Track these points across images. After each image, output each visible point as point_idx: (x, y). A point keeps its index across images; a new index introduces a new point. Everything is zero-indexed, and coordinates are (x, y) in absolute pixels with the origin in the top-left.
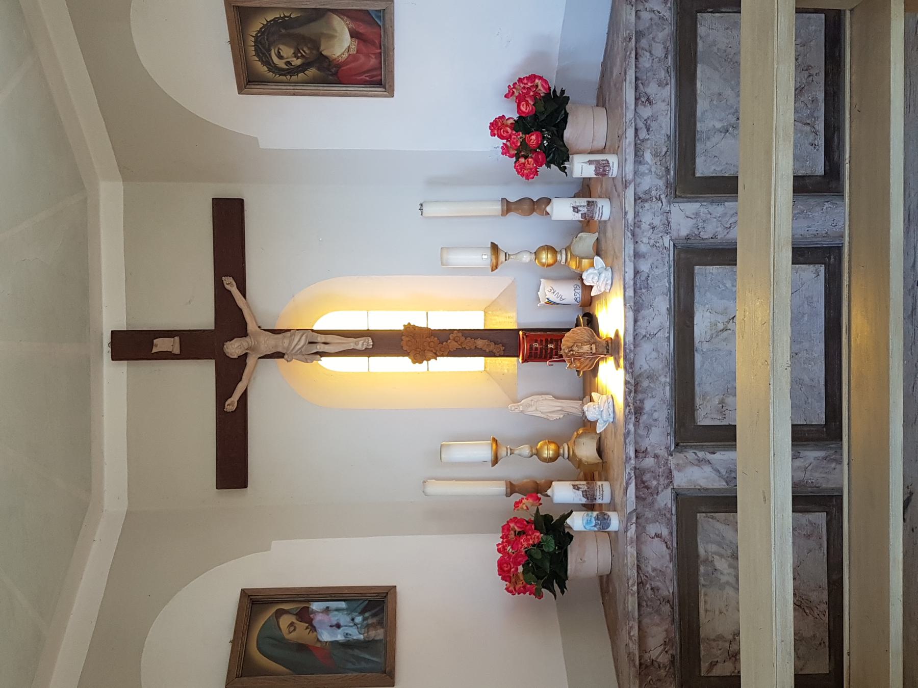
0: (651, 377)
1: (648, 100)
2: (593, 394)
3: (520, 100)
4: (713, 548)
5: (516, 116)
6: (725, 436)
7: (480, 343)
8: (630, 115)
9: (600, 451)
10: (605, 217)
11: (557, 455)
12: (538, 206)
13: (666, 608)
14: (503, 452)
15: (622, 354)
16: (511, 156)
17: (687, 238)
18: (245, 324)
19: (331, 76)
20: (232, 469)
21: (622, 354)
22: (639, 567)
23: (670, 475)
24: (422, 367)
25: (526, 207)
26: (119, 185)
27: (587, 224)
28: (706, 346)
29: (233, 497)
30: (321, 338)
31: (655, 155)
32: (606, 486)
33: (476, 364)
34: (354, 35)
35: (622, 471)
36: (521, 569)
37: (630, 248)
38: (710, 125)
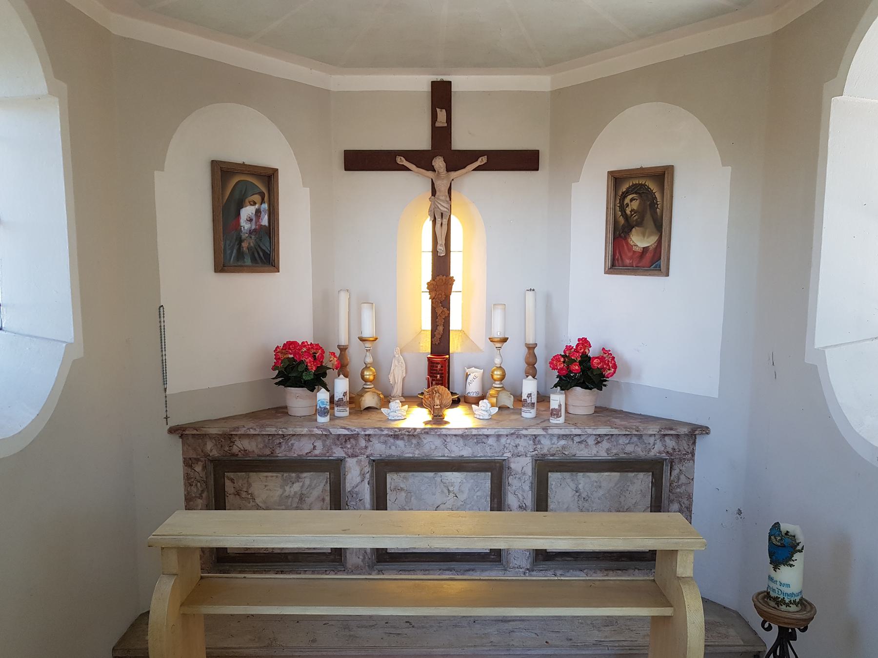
0: (419, 445)
1: (599, 442)
2: (407, 406)
3: (601, 359)
4: (307, 482)
5: (590, 355)
6: (380, 503)
7: (441, 328)
8: (590, 431)
9: (368, 409)
10: (524, 414)
11: (366, 380)
12: (531, 370)
13: (268, 452)
14: (368, 345)
15: (434, 426)
16: (565, 352)
17: (509, 468)
18: (455, 170)
19: (619, 233)
20: (358, 161)
21: (434, 426)
22: (294, 435)
23: (353, 456)
24: (424, 287)
25: (531, 360)
26: (548, 89)
27: (518, 399)
28: (438, 479)
29: (339, 161)
30: (445, 221)
31: (563, 447)
32: (346, 414)
33: (426, 323)
34: (645, 249)
35: (356, 425)
36: (291, 356)
37: (503, 432)
38: (581, 482)
